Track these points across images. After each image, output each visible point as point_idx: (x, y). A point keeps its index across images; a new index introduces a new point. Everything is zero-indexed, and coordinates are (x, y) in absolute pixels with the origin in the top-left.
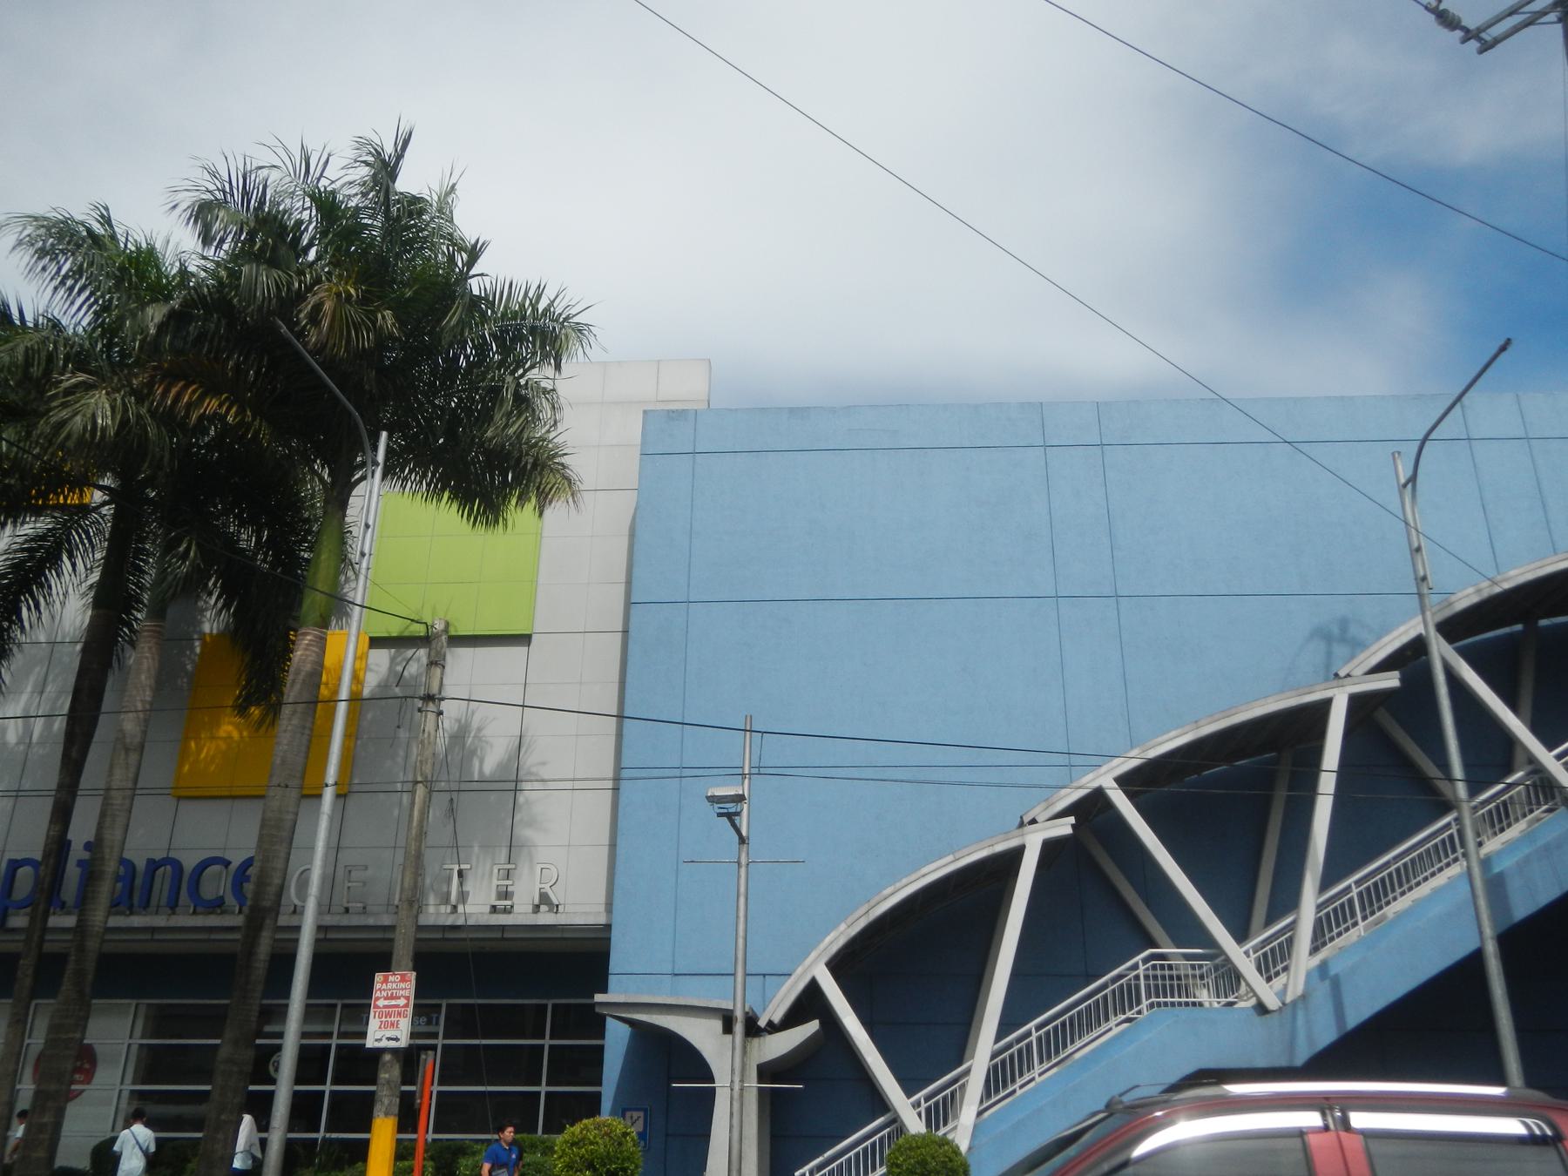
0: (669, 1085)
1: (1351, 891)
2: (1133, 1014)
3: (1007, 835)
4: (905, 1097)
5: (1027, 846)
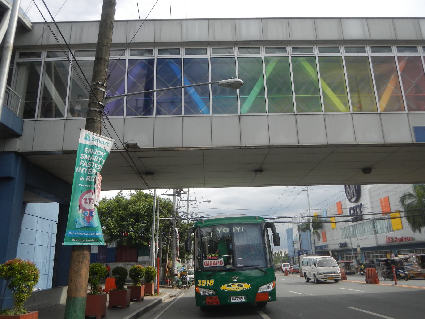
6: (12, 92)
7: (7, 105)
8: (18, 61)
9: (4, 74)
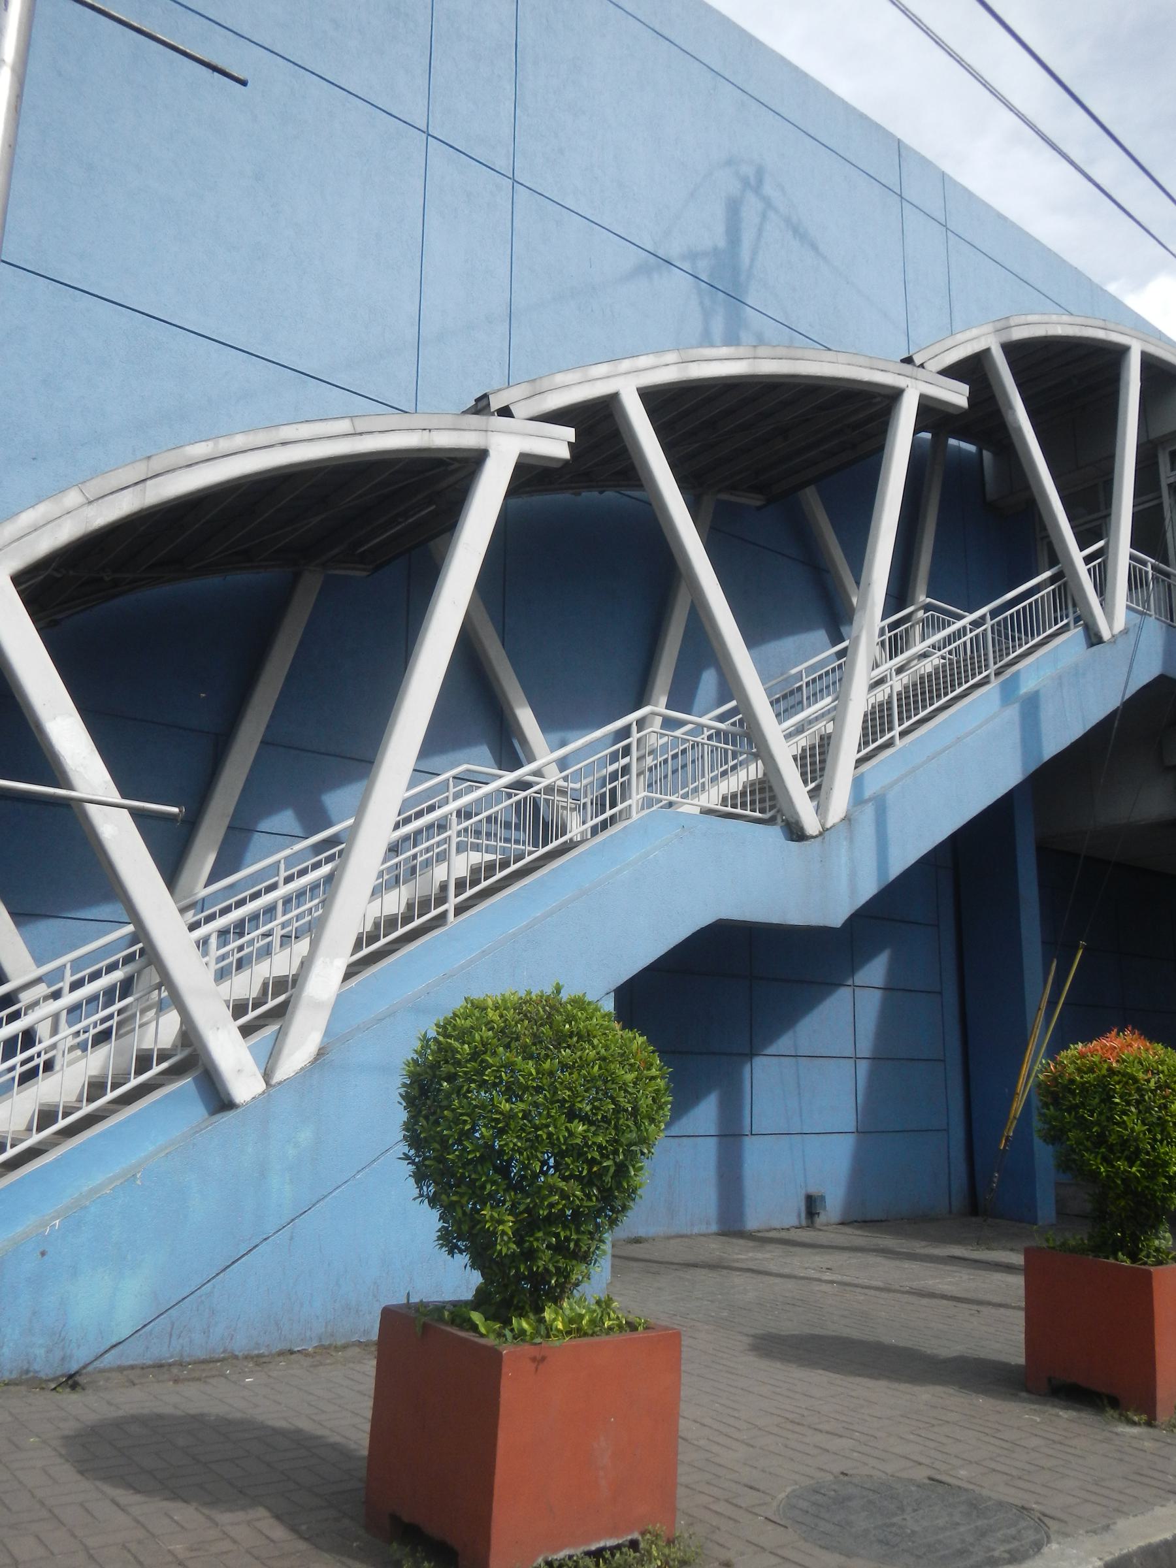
5: (492, 452)
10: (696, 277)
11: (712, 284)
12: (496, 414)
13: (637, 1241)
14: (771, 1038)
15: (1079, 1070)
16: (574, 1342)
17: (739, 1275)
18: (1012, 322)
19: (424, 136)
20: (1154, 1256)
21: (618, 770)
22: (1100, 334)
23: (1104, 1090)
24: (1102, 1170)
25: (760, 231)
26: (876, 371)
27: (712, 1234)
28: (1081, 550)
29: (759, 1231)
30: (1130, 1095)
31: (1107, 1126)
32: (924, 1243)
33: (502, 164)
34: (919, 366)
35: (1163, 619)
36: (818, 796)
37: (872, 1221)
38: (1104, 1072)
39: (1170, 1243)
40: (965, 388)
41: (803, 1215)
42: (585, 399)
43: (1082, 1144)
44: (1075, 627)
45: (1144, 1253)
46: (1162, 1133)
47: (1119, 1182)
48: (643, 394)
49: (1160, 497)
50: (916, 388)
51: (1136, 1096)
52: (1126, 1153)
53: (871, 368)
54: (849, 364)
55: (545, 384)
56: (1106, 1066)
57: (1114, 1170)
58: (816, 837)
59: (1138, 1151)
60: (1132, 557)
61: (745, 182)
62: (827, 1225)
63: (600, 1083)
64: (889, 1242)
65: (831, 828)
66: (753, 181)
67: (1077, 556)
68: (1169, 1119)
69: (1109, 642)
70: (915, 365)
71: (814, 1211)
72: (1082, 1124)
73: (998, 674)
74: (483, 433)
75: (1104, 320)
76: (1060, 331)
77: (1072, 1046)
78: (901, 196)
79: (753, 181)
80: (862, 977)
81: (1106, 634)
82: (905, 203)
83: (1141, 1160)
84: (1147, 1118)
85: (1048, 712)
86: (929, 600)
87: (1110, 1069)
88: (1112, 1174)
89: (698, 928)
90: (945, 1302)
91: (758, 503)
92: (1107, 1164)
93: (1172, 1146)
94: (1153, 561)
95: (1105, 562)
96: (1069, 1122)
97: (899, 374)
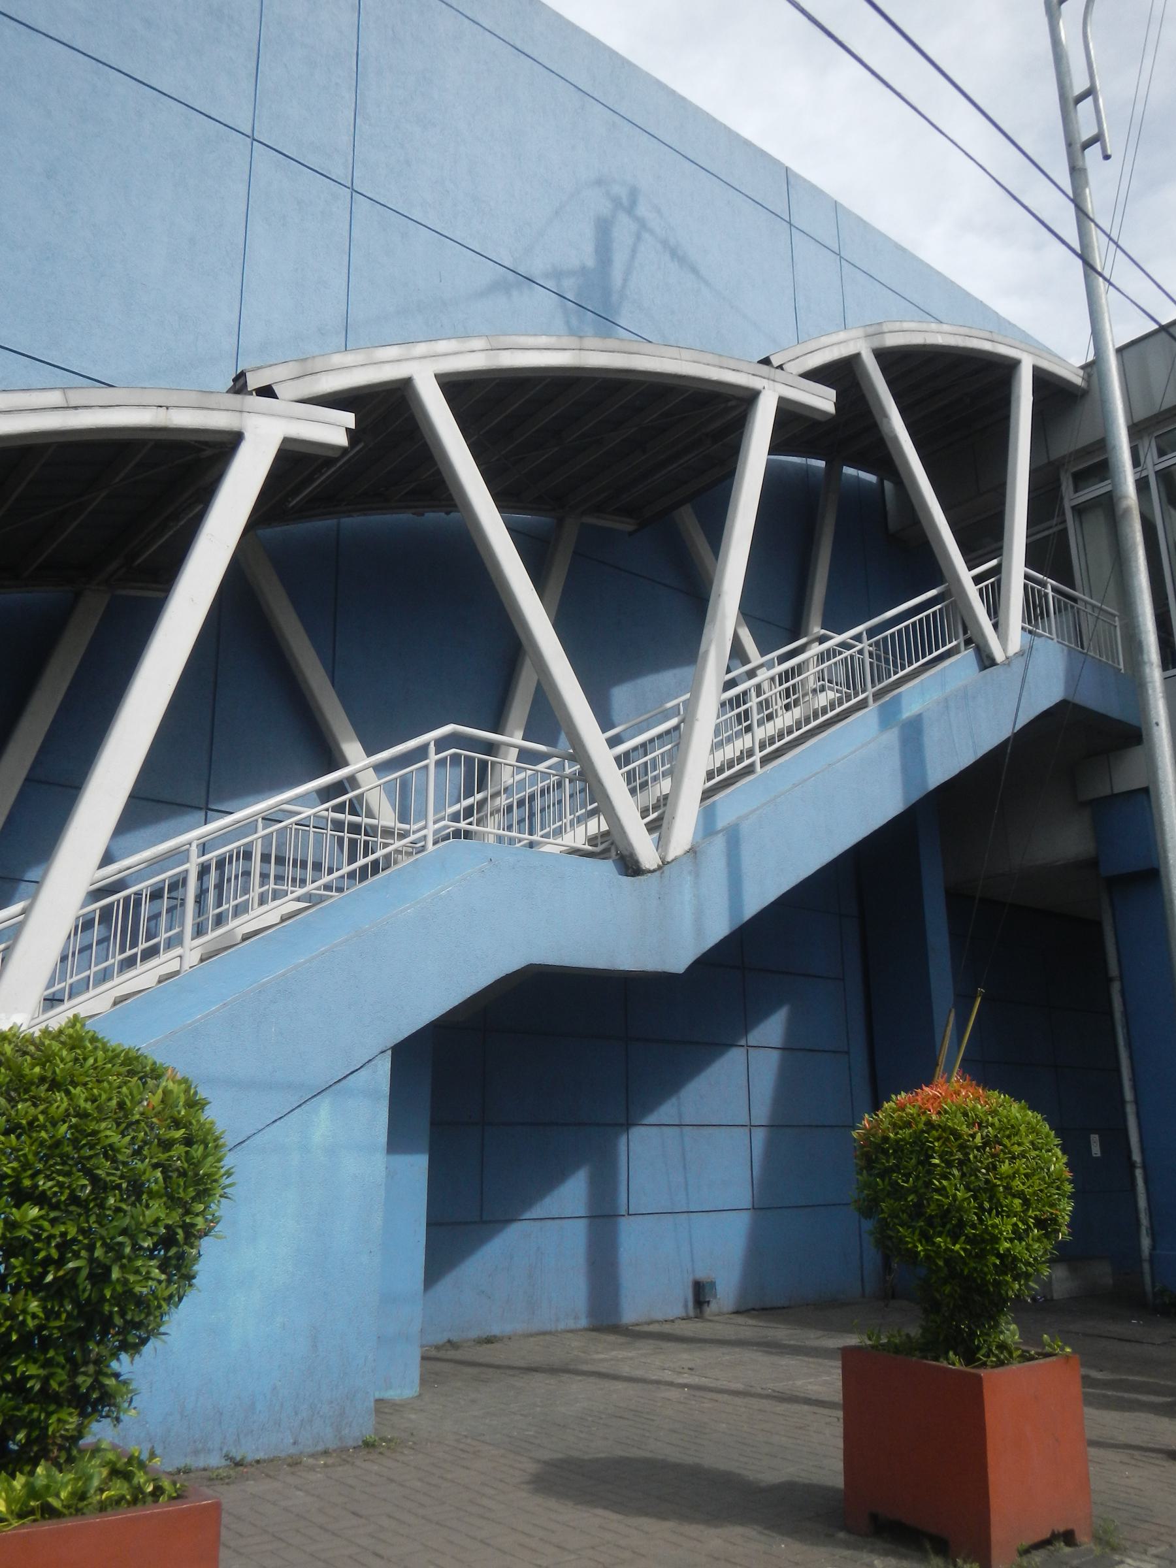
0: (1095, 1131)
1: (436, 832)
2: (318, 888)
3: (204, 401)
4: (383, 1139)
5: (247, 435)
6: (1086, 602)
7: (1082, 647)
8: (1075, 503)
9: (1141, 591)
10: (562, 296)
11: (580, 304)
12: (254, 393)
13: (489, 1340)
14: (650, 1108)
15: (894, 1125)
16: (35, 1528)
17: (580, 1381)
18: (885, 328)
19: (249, 140)
20: (996, 1356)
21: (460, 811)
22: (987, 346)
23: (922, 1149)
24: (920, 1248)
25: (634, 251)
26: (726, 371)
27: (581, 1330)
28: (970, 569)
29: (637, 1325)
30: (952, 1154)
31: (925, 1194)
32: (820, 1333)
33: (338, 172)
34: (777, 368)
35: (1066, 643)
36: (660, 826)
37: (772, 1309)
38: (921, 1126)
39: (1017, 1337)
40: (832, 393)
41: (691, 1304)
42: (370, 383)
43: (897, 1217)
44: (966, 650)
45: (984, 1351)
46: (990, 1201)
47: (941, 1263)
48: (448, 383)
49: (1064, 521)
50: (774, 391)
51: (959, 1155)
52: (948, 1226)
53: (721, 367)
54: (695, 362)
55: (319, 364)
56: (923, 1118)
57: (935, 1249)
58: (654, 871)
59: (961, 1224)
60: (1027, 577)
61: (617, 202)
62: (720, 1314)
63: (68, 1149)
64: (781, 1333)
65: (673, 861)
66: (625, 201)
67: (966, 576)
68: (999, 1183)
69: (1003, 664)
70: (772, 366)
71: (702, 1299)
72: (897, 1192)
73: (877, 696)
74: (238, 414)
75: (991, 332)
76: (940, 340)
77: (893, 1097)
78: (790, 223)
79: (625, 201)
80: (755, 1037)
81: (999, 656)
82: (794, 230)
83: (966, 1235)
84: (971, 1182)
85: (932, 737)
86: (823, 632)
87: (929, 1124)
88: (932, 1254)
89: (502, 975)
90: (806, 1408)
91: (630, 528)
92: (927, 1241)
93: (1002, 1216)
94: (1054, 582)
95: (999, 581)
96: (883, 1190)
97: (754, 375)
